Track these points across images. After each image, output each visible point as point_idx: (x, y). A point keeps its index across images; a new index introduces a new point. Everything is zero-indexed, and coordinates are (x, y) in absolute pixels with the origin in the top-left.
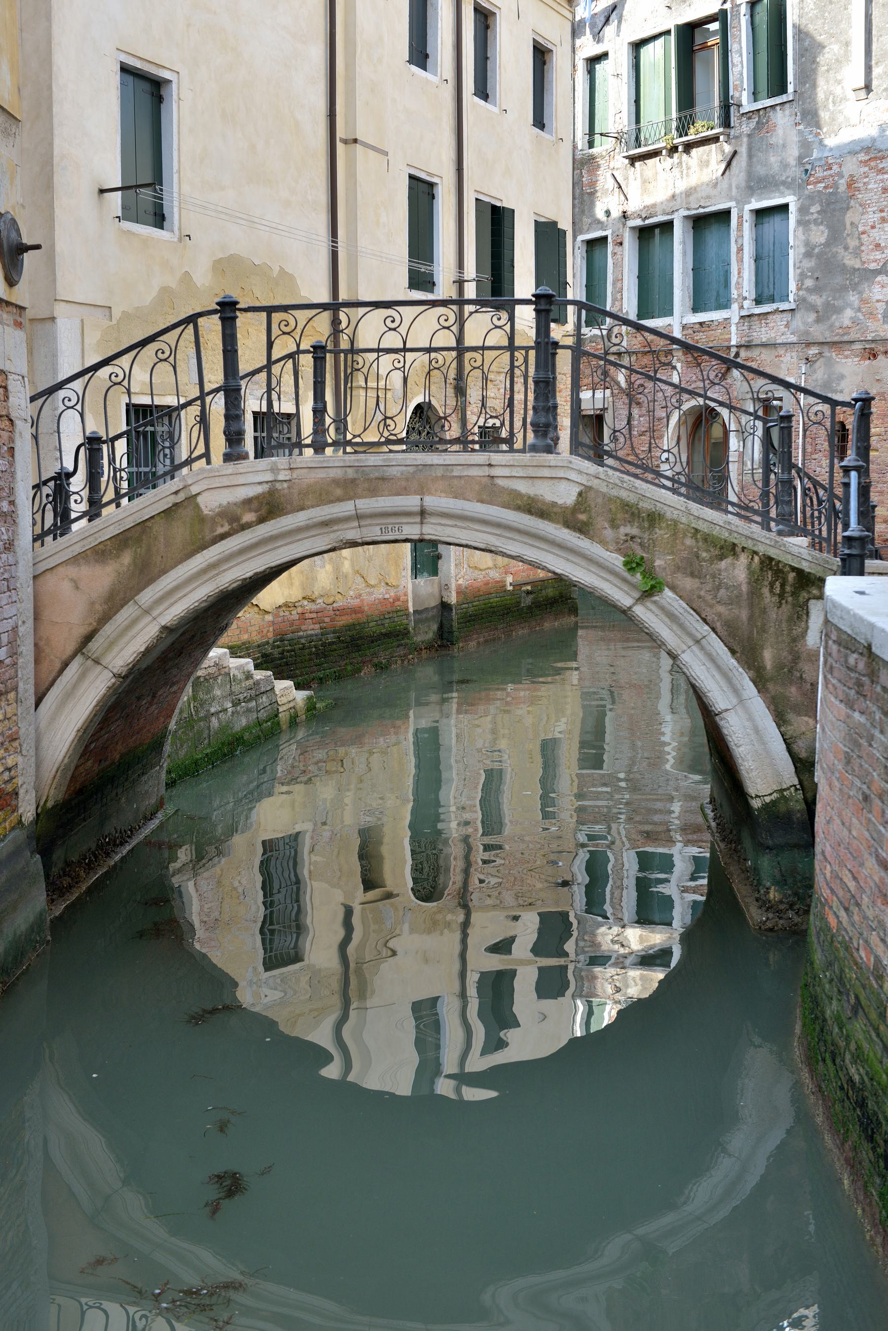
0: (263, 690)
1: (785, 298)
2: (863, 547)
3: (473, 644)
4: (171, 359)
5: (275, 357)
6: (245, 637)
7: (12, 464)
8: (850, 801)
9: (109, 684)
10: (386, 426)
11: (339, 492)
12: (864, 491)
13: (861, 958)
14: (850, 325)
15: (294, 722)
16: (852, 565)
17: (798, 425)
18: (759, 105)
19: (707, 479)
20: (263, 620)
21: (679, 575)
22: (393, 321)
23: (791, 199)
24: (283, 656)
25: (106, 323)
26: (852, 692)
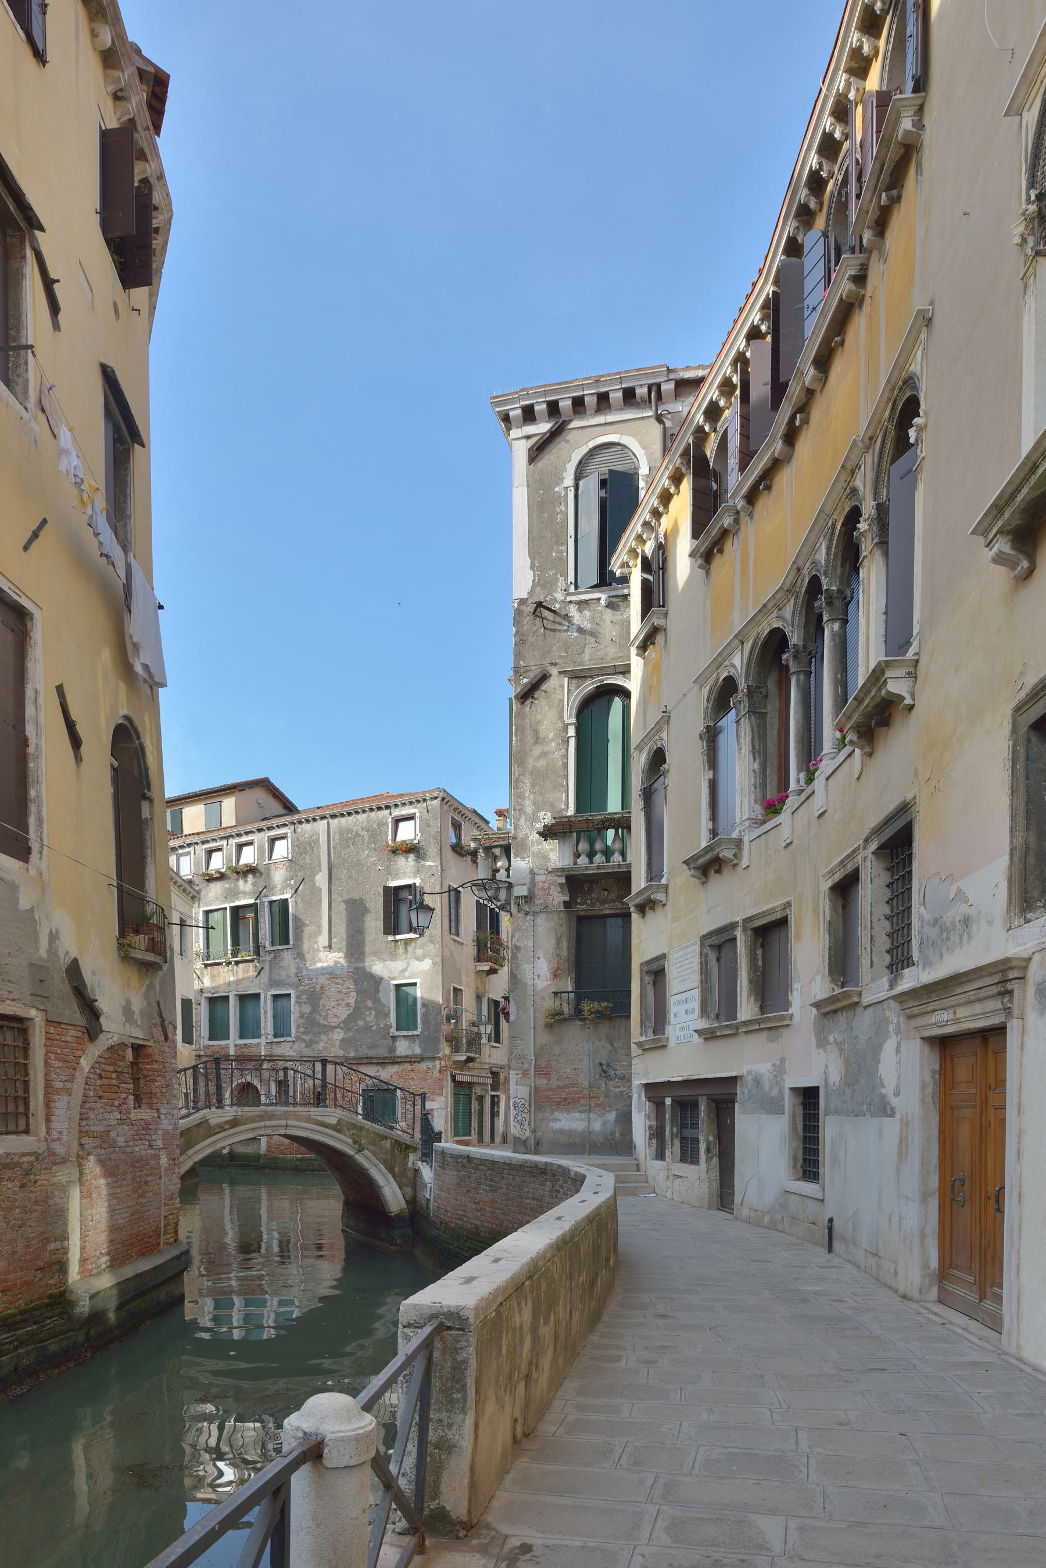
18: (275, 948)
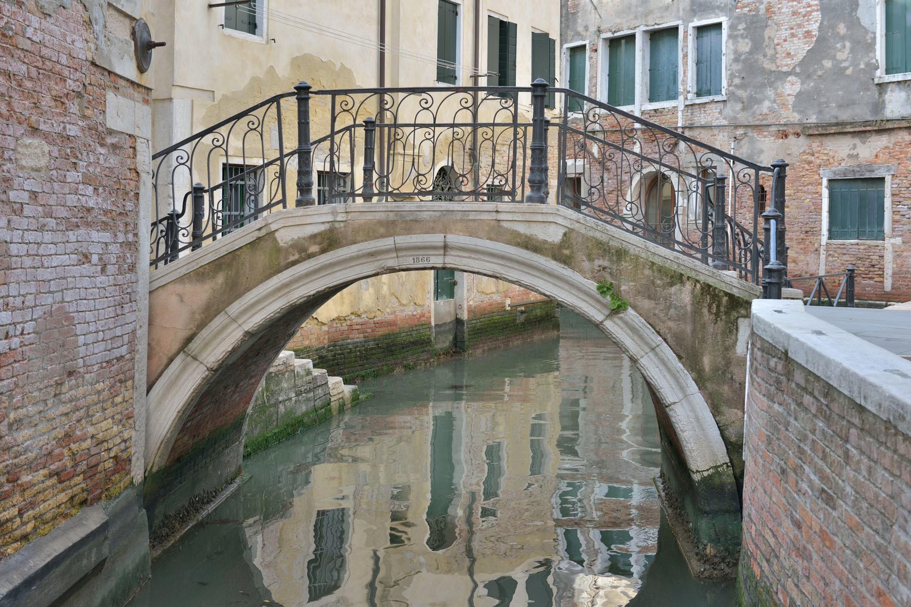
0: (319, 384)
1: (719, 92)
2: (780, 278)
3: (479, 351)
4: (258, 128)
5: (337, 129)
6: (307, 343)
7: (137, 205)
8: (771, 474)
9: (204, 376)
10: (419, 182)
11: (382, 230)
12: (781, 235)
13: (780, 600)
14: (768, 112)
15: (342, 409)
16: (772, 291)
17: (730, 182)
19: (659, 222)
20: (321, 329)
21: (639, 298)
22: (426, 103)
23: (723, 19)
24: (333, 359)
25: (210, 103)
26: (773, 388)
